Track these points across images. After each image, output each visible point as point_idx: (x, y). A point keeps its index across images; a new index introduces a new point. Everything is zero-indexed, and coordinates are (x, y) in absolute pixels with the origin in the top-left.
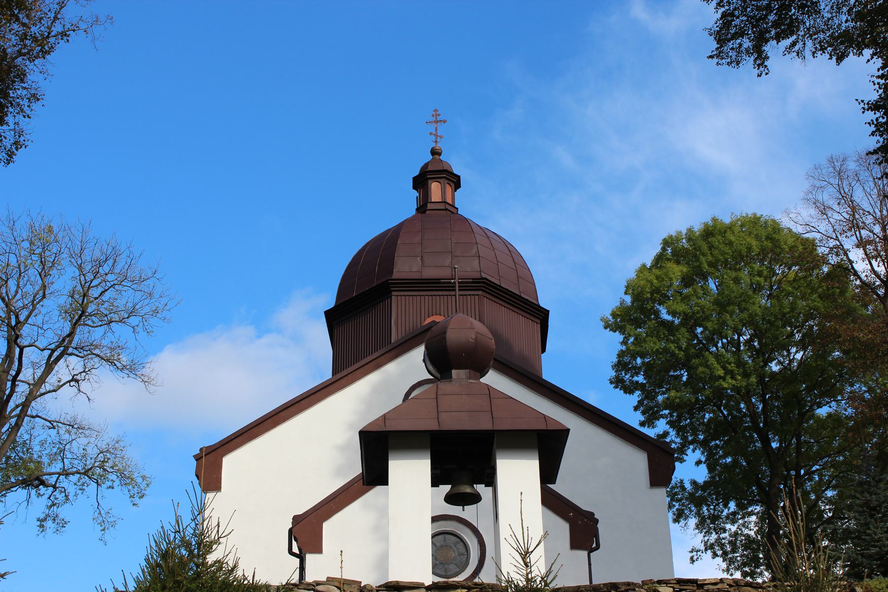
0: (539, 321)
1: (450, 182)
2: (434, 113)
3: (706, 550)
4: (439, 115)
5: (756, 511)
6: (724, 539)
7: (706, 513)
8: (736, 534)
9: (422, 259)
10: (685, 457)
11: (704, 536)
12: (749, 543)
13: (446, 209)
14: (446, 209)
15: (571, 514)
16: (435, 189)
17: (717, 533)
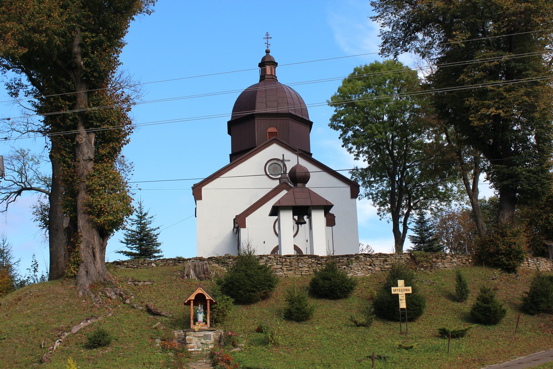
3: (366, 196)
4: (269, 35)
9: (266, 104)
10: (359, 158)
13: (273, 78)
14: (273, 78)
16: (268, 68)
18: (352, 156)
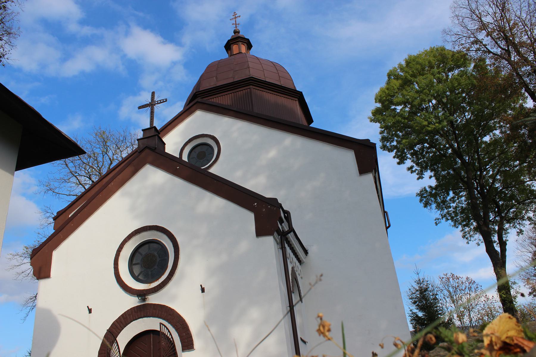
0: (297, 99)
1: (243, 43)
2: (234, 14)
3: (442, 218)
5: (464, 194)
6: (450, 211)
7: (439, 200)
8: (456, 207)
11: (441, 212)
12: (463, 210)
15: (256, 204)
17: (447, 209)
18: (415, 176)
